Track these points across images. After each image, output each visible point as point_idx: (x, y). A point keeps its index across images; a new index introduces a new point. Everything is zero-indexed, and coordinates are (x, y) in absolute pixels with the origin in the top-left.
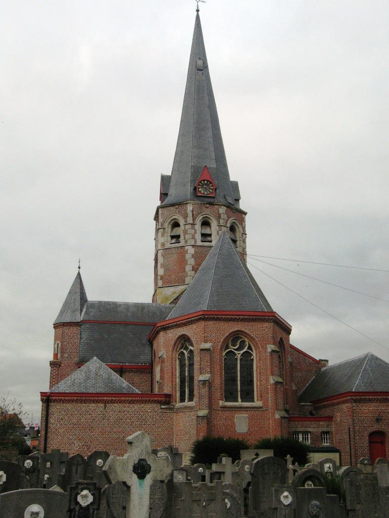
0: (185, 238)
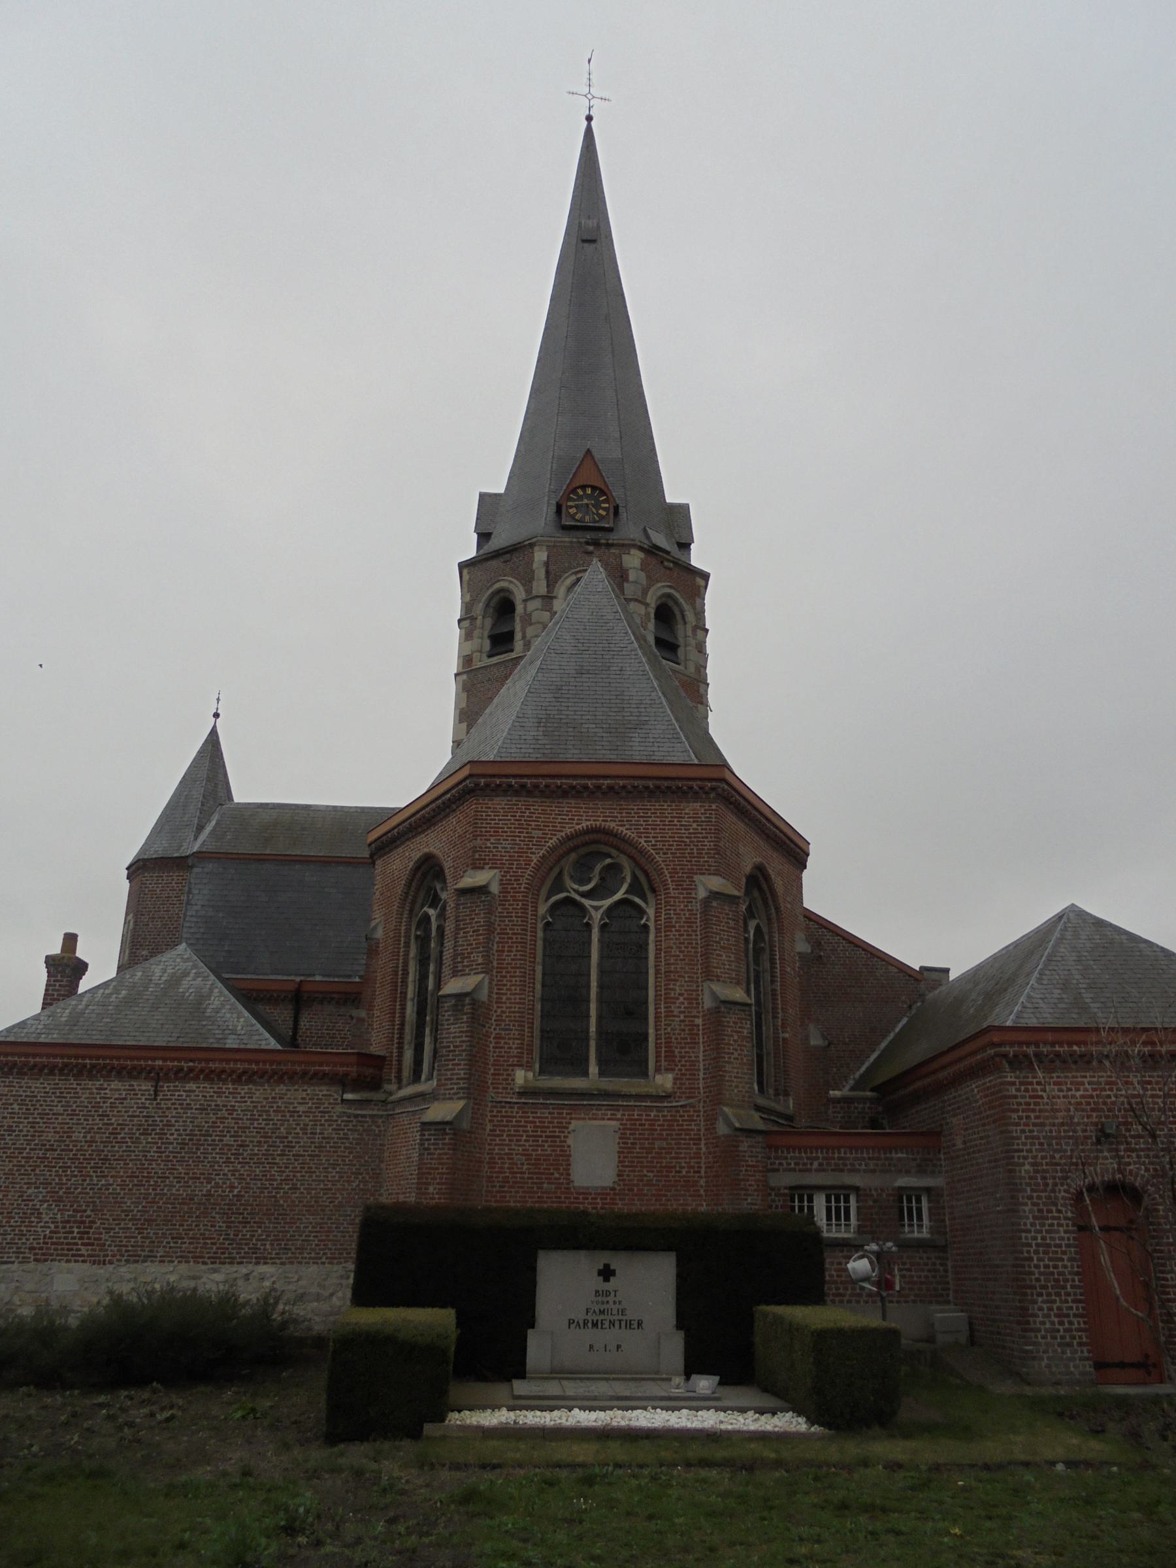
0: (524, 637)
